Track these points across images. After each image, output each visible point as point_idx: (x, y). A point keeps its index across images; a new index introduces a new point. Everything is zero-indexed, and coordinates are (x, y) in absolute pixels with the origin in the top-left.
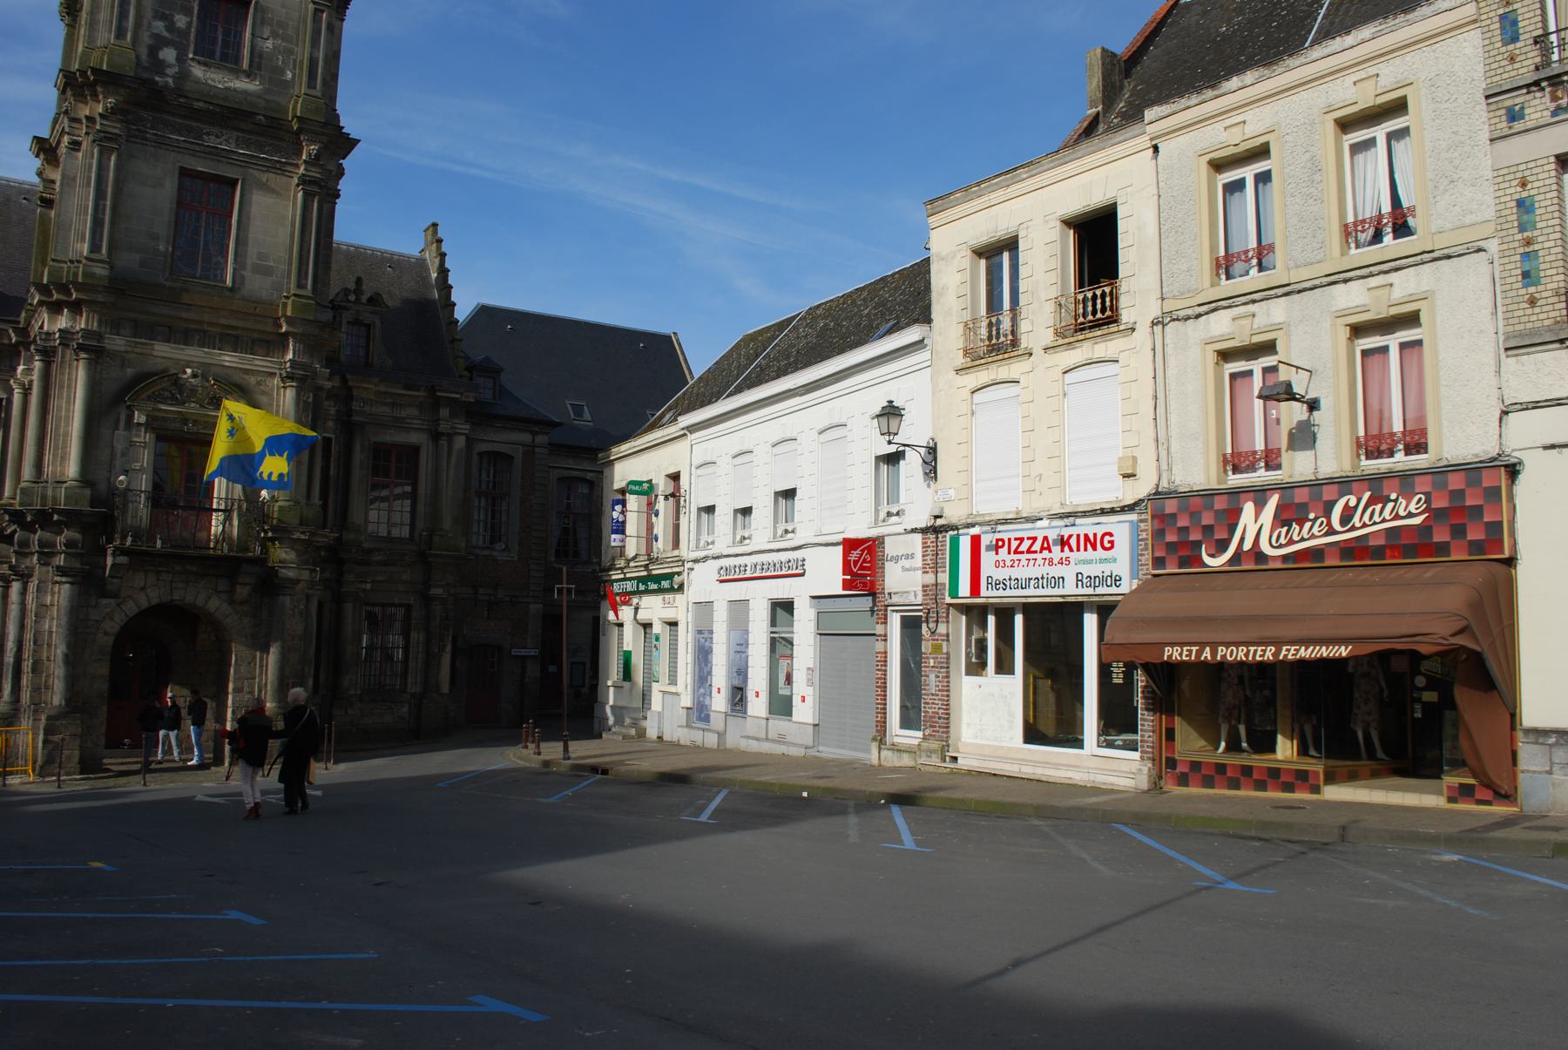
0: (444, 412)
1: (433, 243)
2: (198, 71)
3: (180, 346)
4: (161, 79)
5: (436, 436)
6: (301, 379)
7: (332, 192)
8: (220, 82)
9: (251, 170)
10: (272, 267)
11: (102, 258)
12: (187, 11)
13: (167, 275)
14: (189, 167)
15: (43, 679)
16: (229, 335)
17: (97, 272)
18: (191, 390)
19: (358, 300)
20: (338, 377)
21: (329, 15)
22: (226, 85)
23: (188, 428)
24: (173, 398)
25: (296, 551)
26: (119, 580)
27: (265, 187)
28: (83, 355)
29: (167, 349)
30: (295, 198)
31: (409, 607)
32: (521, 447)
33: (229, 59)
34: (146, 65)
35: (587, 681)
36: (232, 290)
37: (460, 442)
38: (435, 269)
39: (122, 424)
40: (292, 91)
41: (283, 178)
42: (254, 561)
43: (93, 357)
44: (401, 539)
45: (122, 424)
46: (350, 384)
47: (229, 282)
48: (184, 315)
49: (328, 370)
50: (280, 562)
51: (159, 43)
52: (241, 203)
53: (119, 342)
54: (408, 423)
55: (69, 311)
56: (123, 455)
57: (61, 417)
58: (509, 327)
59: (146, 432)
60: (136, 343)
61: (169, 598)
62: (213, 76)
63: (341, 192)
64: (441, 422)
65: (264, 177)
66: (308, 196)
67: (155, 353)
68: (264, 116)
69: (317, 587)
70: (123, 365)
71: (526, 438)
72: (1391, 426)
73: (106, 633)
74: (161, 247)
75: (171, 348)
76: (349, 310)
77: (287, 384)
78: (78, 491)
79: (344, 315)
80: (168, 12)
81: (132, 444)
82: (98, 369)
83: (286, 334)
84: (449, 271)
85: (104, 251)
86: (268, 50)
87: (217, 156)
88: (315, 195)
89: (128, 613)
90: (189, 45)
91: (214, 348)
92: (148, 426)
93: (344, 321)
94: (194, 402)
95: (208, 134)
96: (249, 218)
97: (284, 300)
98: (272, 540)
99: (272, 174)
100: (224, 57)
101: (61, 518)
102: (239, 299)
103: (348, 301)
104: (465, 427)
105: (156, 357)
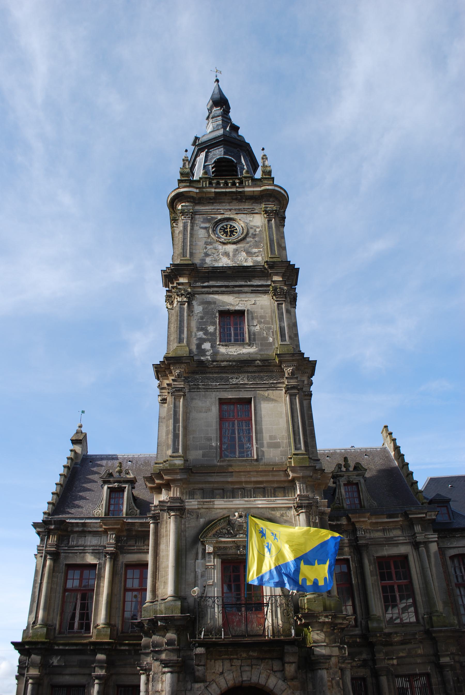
0: (418, 528)
1: (387, 436)
2: (223, 350)
3: (230, 499)
4: (205, 358)
5: (416, 545)
6: (307, 506)
7: (307, 393)
8: (235, 352)
9: (258, 392)
10: (280, 442)
11: (179, 454)
12: (214, 324)
13: (218, 458)
14: (225, 397)
17: (177, 463)
18: (239, 526)
19: (347, 470)
20: (344, 517)
21: (286, 305)
22: (238, 353)
23: (240, 552)
24: (229, 533)
25: (325, 633)
26: (203, 667)
27: (268, 399)
28: (172, 514)
29: (223, 503)
30: (285, 400)
31: (428, 675)
34: (196, 353)
36: (257, 460)
37: (434, 547)
38: (392, 450)
39: (200, 555)
40: (274, 347)
42: (292, 643)
43: (177, 513)
44: (410, 623)
45: (200, 555)
46: (352, 520)
47: (255, 457)
48: (230, 480)
49: (327, 500)
50: (314, 642)
51: (201, 341)
52: (255, 410)
53: (193, 503)
54: (396, 540)
55: (165, 489)
56: (202, 576)
58: (450, 486)
59: (214, 558)
60: (204, 502)
62: (230, 350)
63: (312, 393)
64: (418, 535)
65: (266, 393)
66: (292, 397)
67: (215, 507)
68: (259, 360)
69: (347, 661)
70: (198, 517)
74: (213, 444)
75: (225, 502)
76: (343, 476)
77: (300, 512)
78: (172, 603)
79: (340, 480)
80: (204, 327)
81: (207, 567)
82: (183, 522)
83: (293, 481)
84: (400, 447)
85: (180, 451)
86: (257, 330)
88: (296, 394)
90: (217, 339)
91: (251, 497)
92: (215, 554)
93: (342, 484)
94: (242, 534)
95: (232, 378)
96: (261, 418)
97: (289, 460)
98: (306, 625)
99: (270, 391)
100: (236, 340)
101: (162, 624)
102: (262, 465)
103: (341, 471)
104: (435, 537)
105: (217, 508)
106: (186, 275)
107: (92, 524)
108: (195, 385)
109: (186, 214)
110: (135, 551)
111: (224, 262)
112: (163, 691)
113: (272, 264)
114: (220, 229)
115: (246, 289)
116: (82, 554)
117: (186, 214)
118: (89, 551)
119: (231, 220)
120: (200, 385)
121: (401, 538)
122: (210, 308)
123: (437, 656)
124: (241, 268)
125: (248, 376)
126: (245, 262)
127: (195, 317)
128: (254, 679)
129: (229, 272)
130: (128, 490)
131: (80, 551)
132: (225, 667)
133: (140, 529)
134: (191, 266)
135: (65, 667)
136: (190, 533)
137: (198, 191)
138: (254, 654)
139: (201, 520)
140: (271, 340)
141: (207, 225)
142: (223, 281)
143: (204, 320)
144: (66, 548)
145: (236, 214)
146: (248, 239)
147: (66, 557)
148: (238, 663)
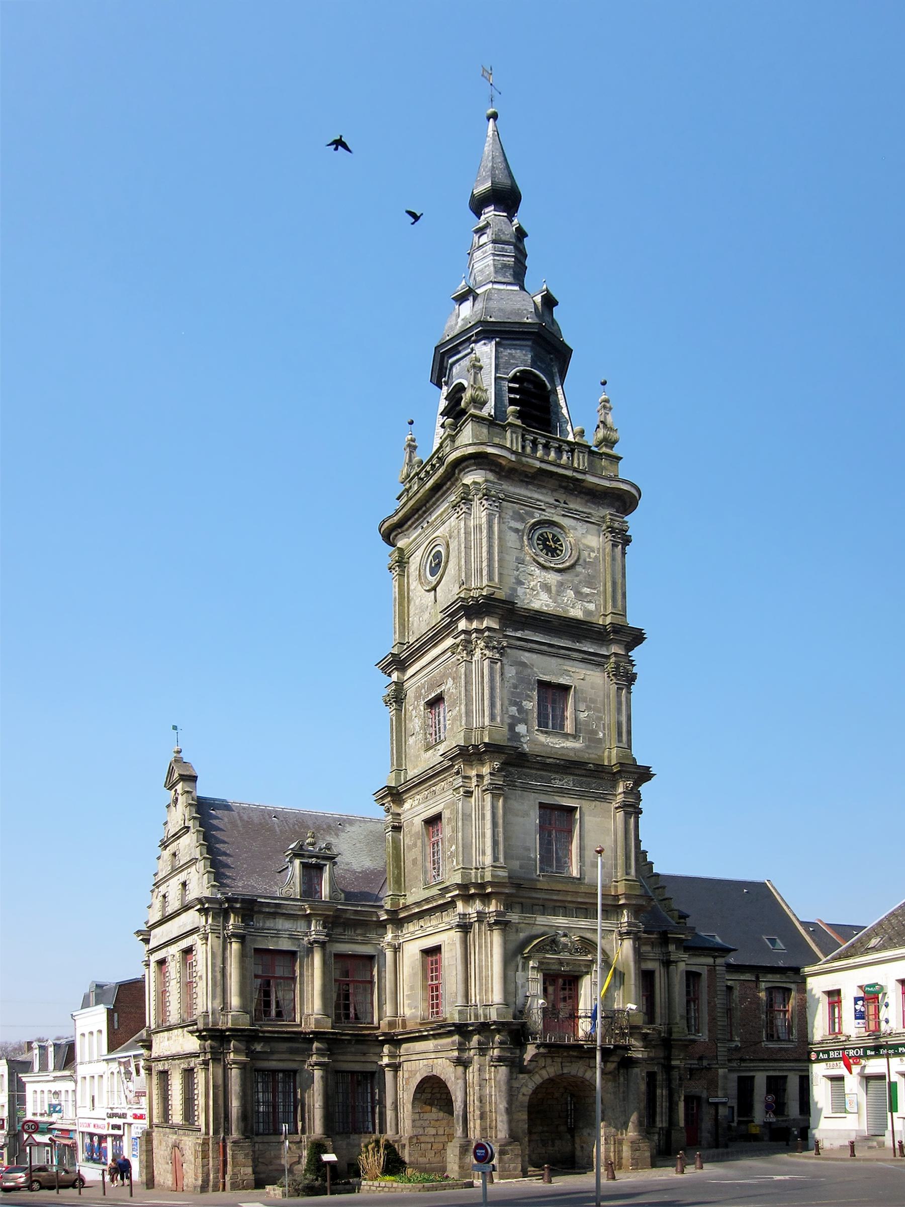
0: (672, 948)
15: (488, 1124)
16: (581, 908)
29: (545, 920)
32: (706, 967)
33: (558, 728)
35: (735, 1118)
41: (605, 804)
53: (514, 917)
54: (645, 956)
56: (522, 987)
57: (482, 966)
61: (561, 1072)
62: (552, 740)
67: (537, 923)
70: (517, 931)
71: (710, 961)
72: (504, 877)
73: (524, 1095)
74: (532, 855)
80: (518, 700)
87: (561, 793)
89: (536, 1082)
106: (496, 616)
107: (289, 906)
108: (512, 781)
109: (494, 499)
110: (346, 940)
111: (541, 602)
112: (491, 1079)
113: (619, 628)
114: (538, 539)
115: (575, 655)
116: (275, 939)
117: (494, 499)
118: (284, 936)
119: (556, 526)
120: (518, 782)
121: (651, 954)
122: (525, 673)
123: (668, 1058)
124: (575, 621)
125: (573, 779)
126: (572, 607)
127: (506, 682)
128: (574, 1072)
129: (556, 623)
130: (329, 867)
131: (271, 935)
132: (547, 1063)
133: (352, 917)
134: (508, 605)
135: (272, 1053)
136: (512, 946)
137: (513, 458)
138: (574, 1054)
139: (521, 934)
140: (601, 735)
141: (520, 526)
142: (543, 634)
143: (518, 690)
144: (253, 930)
145: (563, 515)
146: (579, 569)
147: (255, 941)
148: (560, 1060)
